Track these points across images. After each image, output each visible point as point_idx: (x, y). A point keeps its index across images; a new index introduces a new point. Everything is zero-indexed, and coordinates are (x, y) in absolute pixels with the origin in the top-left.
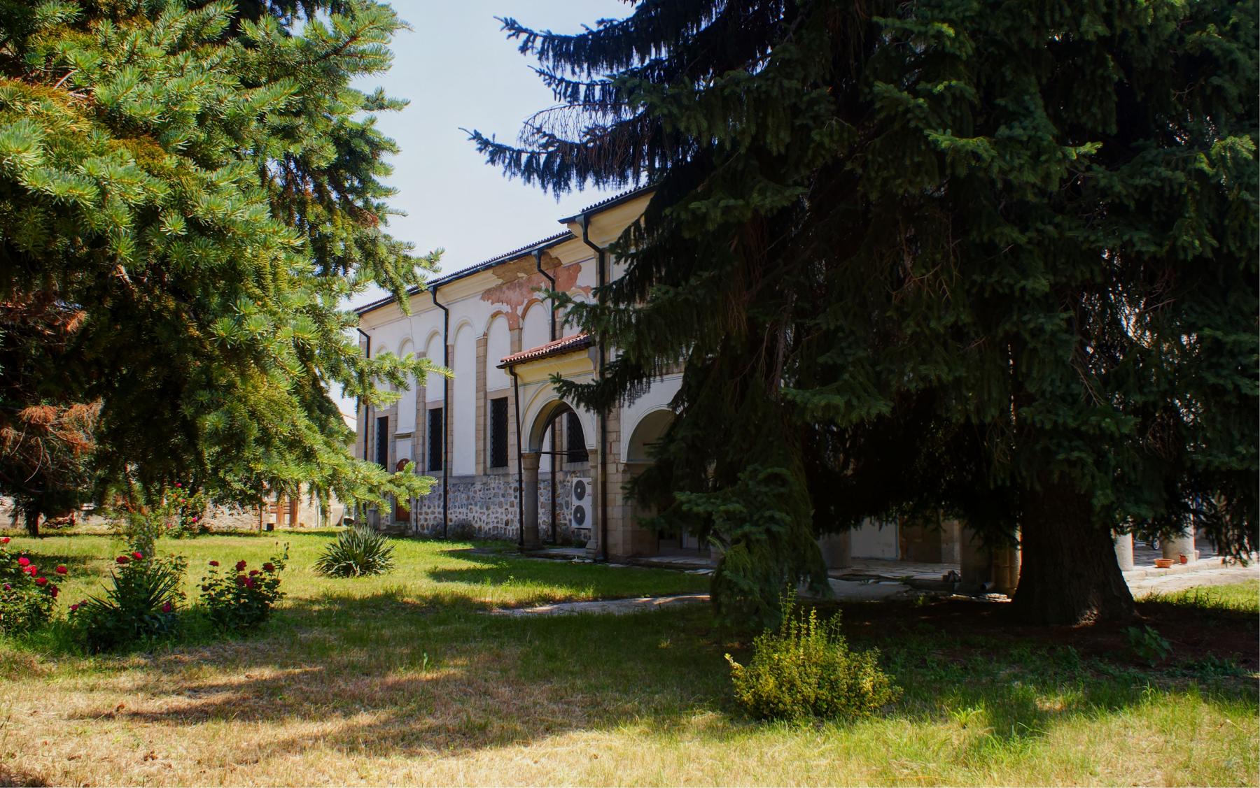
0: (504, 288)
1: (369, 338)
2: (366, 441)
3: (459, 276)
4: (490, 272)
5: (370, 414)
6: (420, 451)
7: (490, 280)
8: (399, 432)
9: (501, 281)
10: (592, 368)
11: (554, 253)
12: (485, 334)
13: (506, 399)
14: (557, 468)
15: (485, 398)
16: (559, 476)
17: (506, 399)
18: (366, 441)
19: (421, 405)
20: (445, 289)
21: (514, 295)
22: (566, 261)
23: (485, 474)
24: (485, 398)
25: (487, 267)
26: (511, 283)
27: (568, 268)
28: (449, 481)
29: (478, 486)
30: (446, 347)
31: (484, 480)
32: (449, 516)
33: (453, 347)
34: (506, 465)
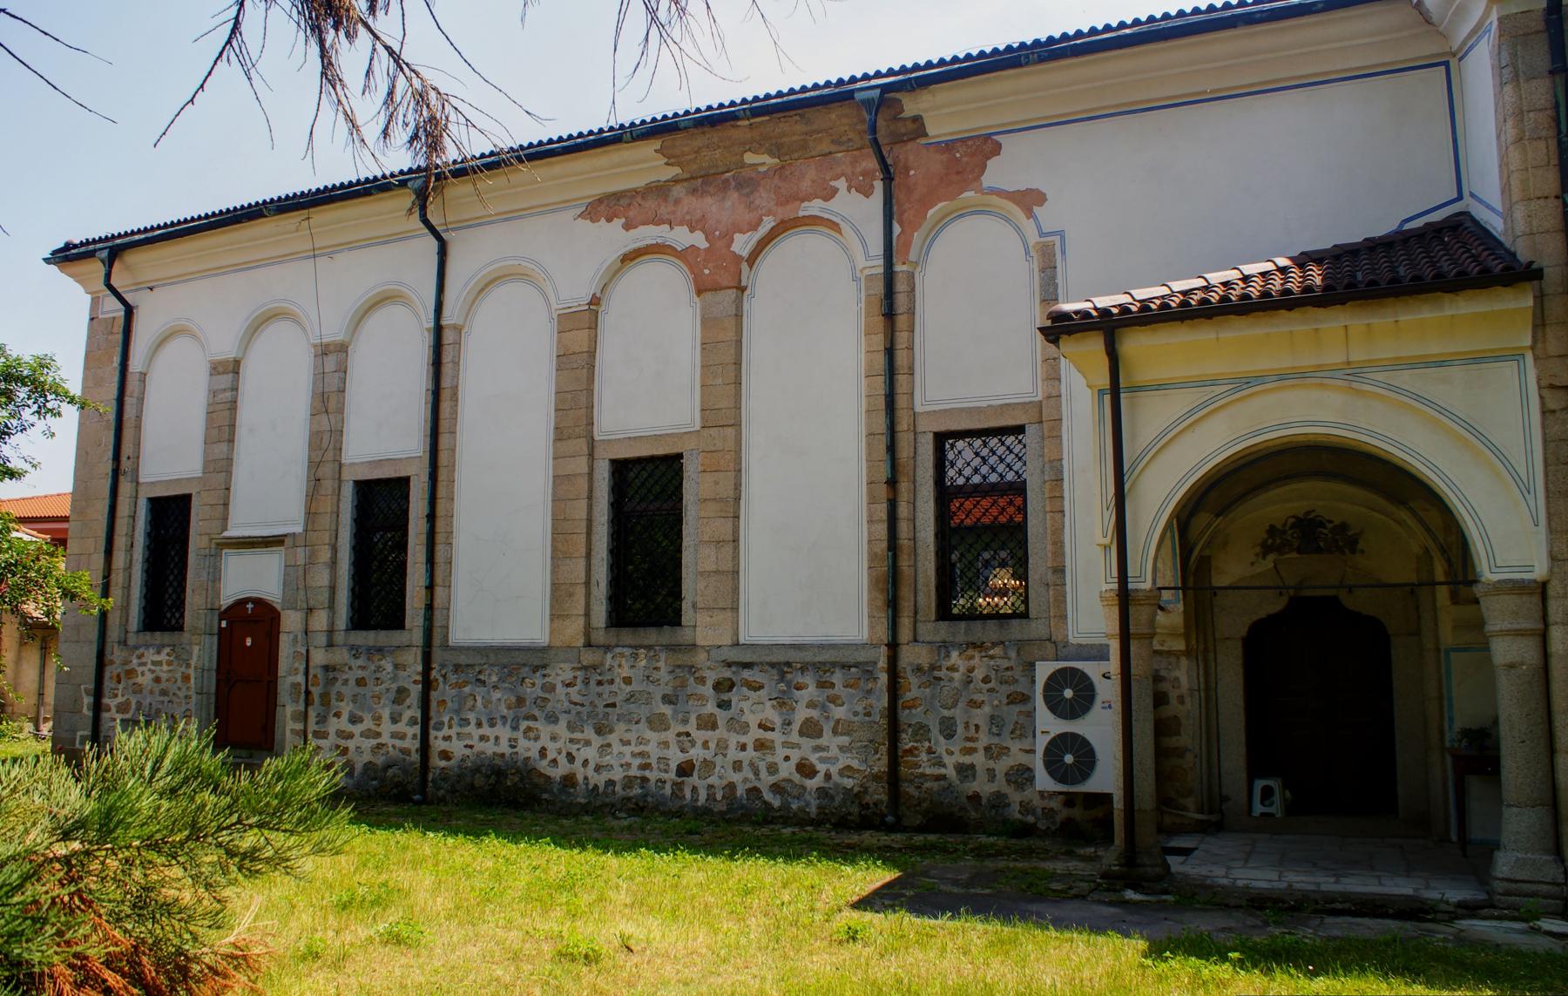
0: (678, 191)
1: (129, 311)
2: (109, 552)
3: (494, 163)
4: (649, 148)
5: (125, 488)
6: (321, 578)
7: (646, 166)
8: (233, 532)
9: (675, 171)
10: (1528, 342)
11: (911, 105)
12: (595, 301)
13: (404, 482)
14: (905, 634)
15: (591, 455)
16: (911, 655)
17: (404, 482)
18: (109, 552)
19: (327, 470)
20: (132, 257)
21: (721, 208)
22: (938, 129)
23: (588, 645)
24: (591, 455)
25: (661, 129)
26: (704, 180)
27: (949, 146)
28: (438, 655)
29: (562, 672)
30: (438, 330)
31: (588, 657)
32: (438, 744)
33: (458, 329)
34: (675, 620)
